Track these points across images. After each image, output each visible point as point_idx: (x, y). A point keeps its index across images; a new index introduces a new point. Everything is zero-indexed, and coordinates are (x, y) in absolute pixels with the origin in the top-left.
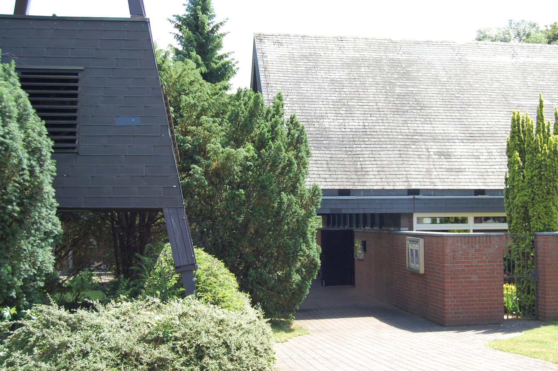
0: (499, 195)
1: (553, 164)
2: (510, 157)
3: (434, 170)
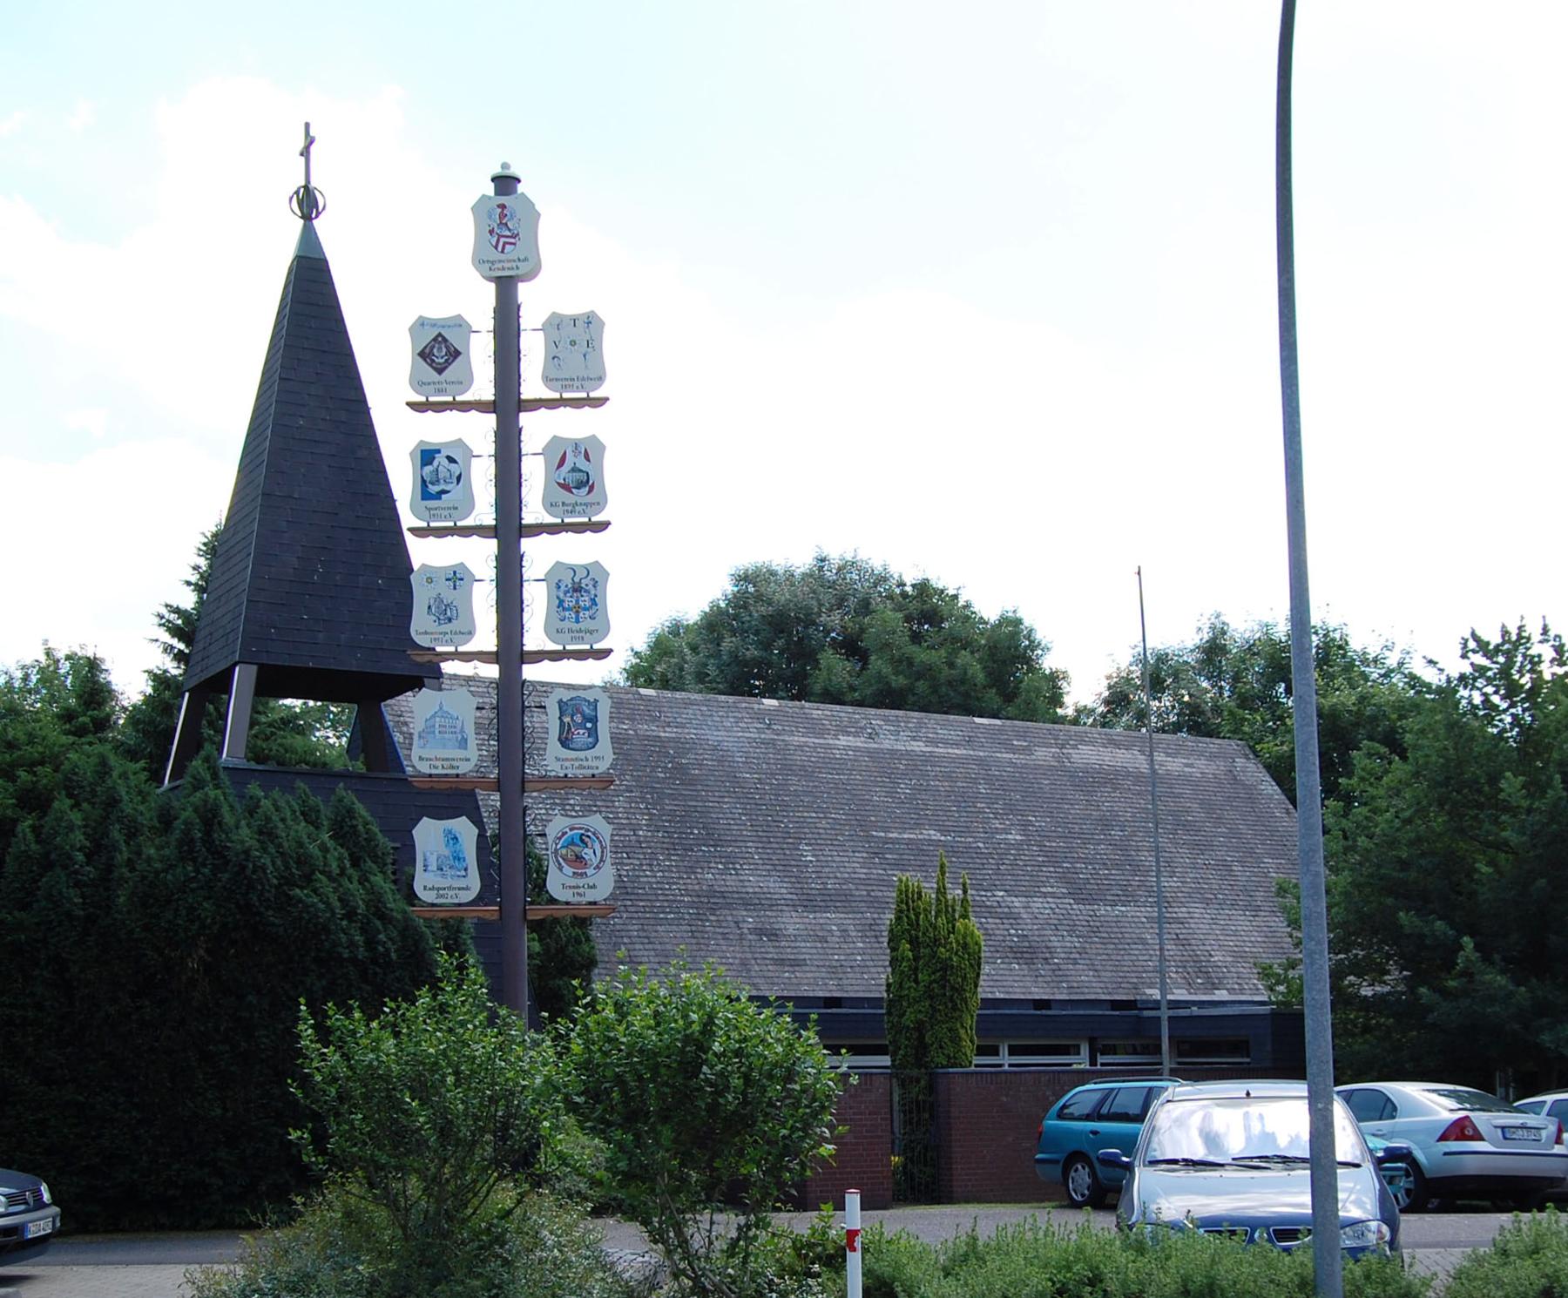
0: (864, 1008)
1: (963, 966)
2: (893, 949)
3: (753, 962)
